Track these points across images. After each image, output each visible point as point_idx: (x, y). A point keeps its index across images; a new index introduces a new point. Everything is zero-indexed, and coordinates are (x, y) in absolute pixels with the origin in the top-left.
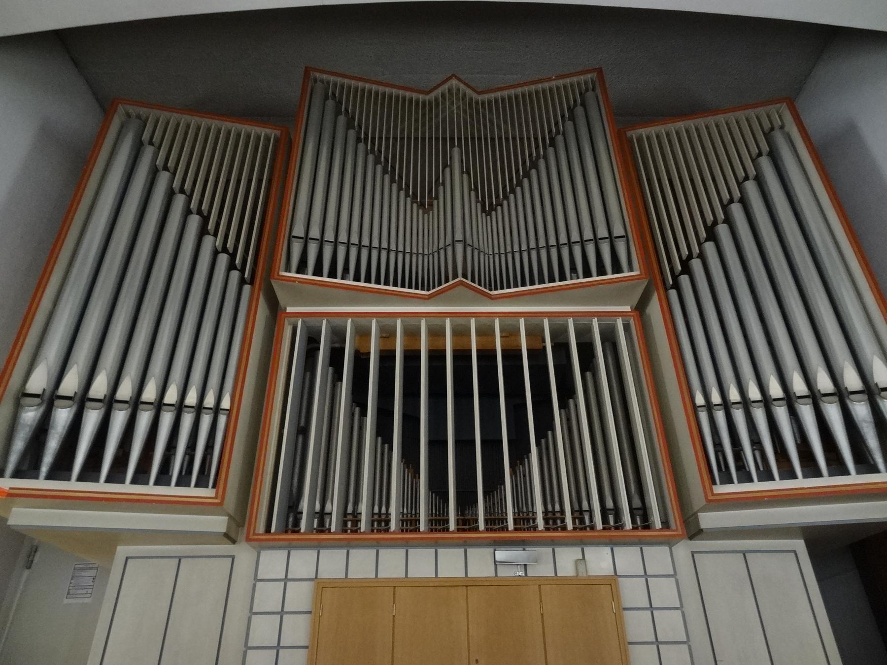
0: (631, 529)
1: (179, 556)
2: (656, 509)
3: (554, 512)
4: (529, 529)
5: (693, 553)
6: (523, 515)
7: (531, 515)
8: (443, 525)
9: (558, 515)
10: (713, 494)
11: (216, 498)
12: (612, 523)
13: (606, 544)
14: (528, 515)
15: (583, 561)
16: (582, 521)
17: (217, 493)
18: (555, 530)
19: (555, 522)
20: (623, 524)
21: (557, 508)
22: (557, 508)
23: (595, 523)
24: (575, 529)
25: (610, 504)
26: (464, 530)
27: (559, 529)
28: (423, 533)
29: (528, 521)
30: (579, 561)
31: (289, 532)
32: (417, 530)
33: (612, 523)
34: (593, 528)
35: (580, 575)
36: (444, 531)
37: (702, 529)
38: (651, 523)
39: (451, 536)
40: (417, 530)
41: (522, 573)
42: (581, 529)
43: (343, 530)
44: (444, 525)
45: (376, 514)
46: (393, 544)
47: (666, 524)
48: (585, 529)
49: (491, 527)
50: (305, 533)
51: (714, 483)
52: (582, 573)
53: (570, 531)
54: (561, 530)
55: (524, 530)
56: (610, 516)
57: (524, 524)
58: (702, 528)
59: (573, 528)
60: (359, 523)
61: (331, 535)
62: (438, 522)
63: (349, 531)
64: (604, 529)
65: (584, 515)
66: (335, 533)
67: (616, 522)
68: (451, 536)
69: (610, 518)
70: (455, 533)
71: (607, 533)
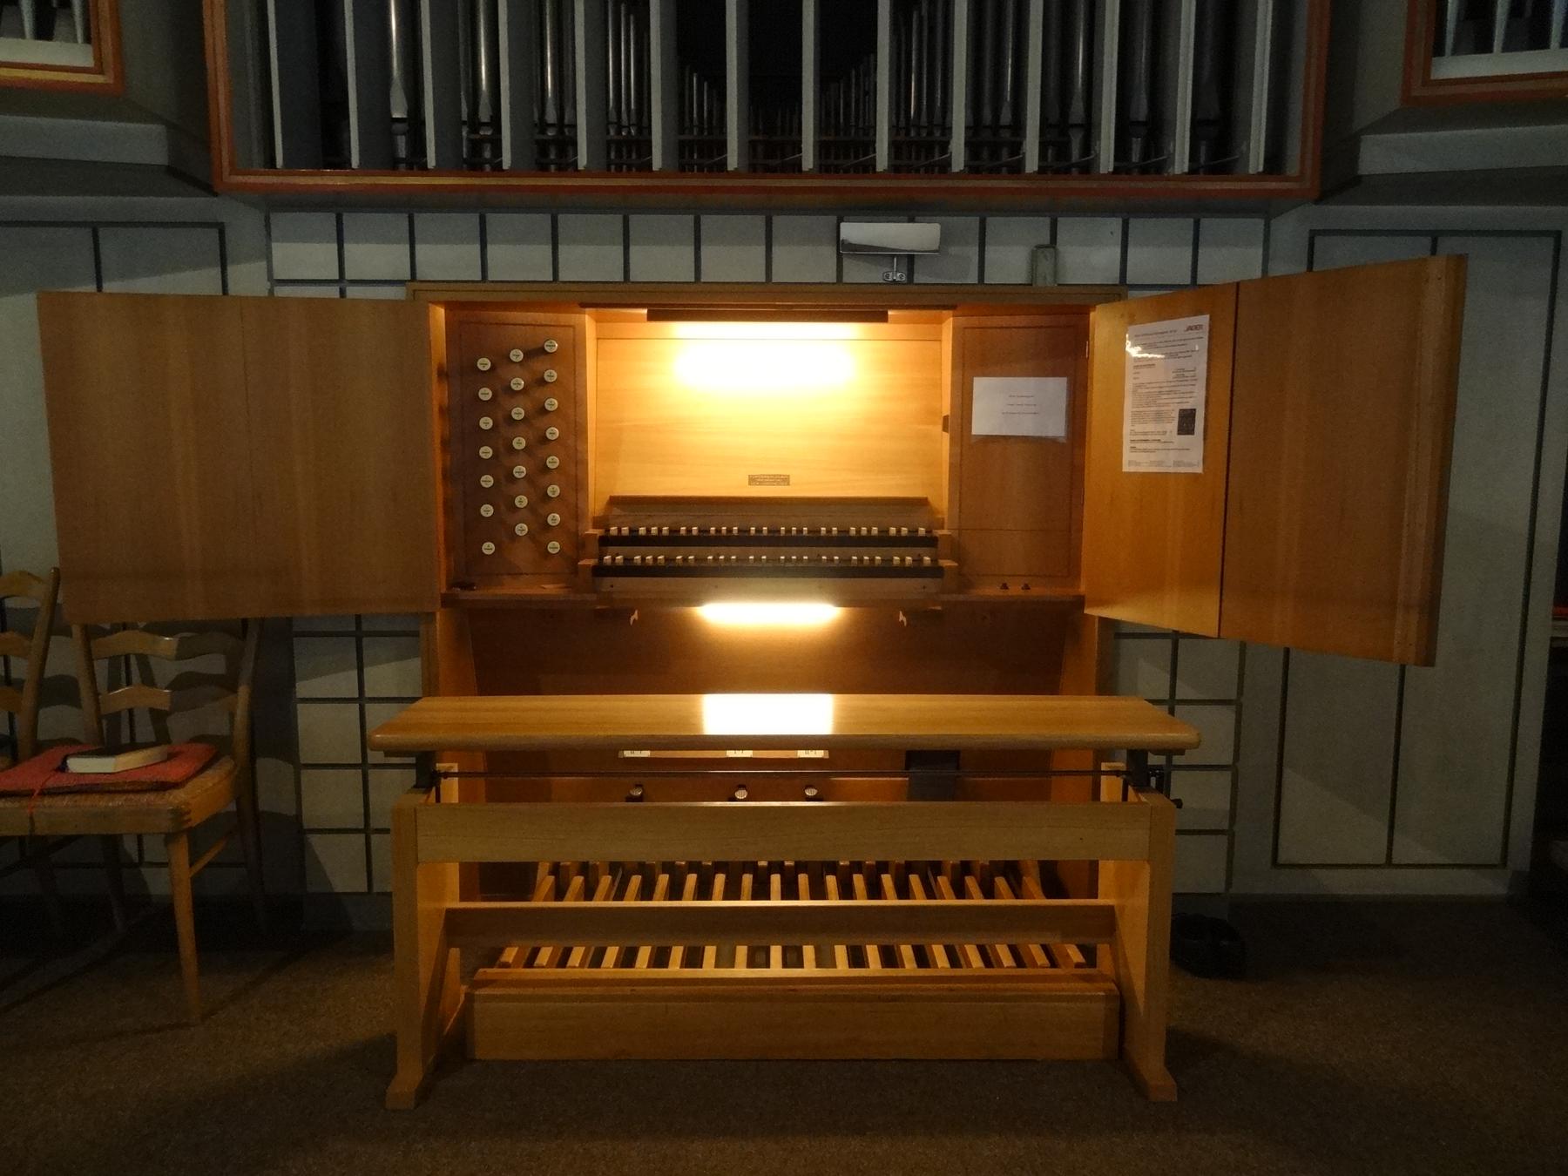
0: (1259, 173)
1: (93, 222)
2: (1266, 26)
3: (996, 127)
4: (929, 170)
5: (1313, 235)
6: (918, 134)
7: (937, 134)
8: (856, 157)
9: (1006, 135)
10: (1427, 82)
11: (99, 69)
12: (1135, 157)
13: (1112, 212)
14: (930, 133)
15: (1052, 250)
16: (1063, 150)
17: (99, 58)
18: (994, 171)
19: (995, 155)
20: (1165, 160)
21: (1006, 117)
22: (1006, 117)
23: (1098, 156)
24: (1042, 170)
25: (1141, 110)
26: (770, 170)
27: (1004, 169)
28: (736, 174)
29: (930, 154)
30: (1040, 251)
31: (402, 166)
32: (871, 168)
33: (1135, 157)
34: (1087, 168)
35: (1040, 282)
36: (711, 170)
37: (1361, 176)
38: (1236, 160)
39: (881, 183)
40: (871, 168)
41: (899, 276)
42: (1057, 172)
43: (821, 165)
44: (859, 158)
45: (553, 125)
46: (588, 203)
47: (1275, 161)
48: (1067, 171)
49: (836, 162)
50: (587, 173)
51: (1439, 50)
52: (1045, 278)
53: (1030, 177)
54: (1081, 173)
55: (917, 171)
56: (1134, 139)
57: (918, 158)
58: (1360, 172)
59: (1039, 167)
60: (570, 149)
61: (652, 178)
62: (687, 149)
63: (553, 167)
64: (1116, 171)
65: (1069, 136)
66: (511, 173)
67: (1146, 155)
68: (881, 183)
69: (1134, 146)
70: (812, 177)
71: (1124, 184)
